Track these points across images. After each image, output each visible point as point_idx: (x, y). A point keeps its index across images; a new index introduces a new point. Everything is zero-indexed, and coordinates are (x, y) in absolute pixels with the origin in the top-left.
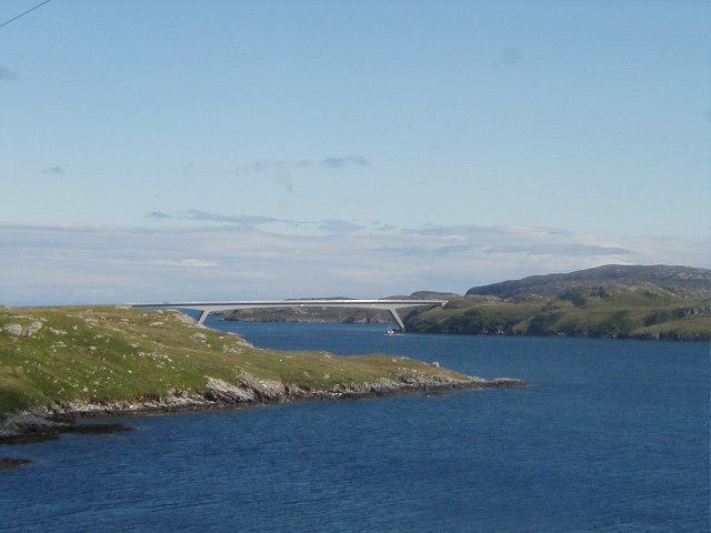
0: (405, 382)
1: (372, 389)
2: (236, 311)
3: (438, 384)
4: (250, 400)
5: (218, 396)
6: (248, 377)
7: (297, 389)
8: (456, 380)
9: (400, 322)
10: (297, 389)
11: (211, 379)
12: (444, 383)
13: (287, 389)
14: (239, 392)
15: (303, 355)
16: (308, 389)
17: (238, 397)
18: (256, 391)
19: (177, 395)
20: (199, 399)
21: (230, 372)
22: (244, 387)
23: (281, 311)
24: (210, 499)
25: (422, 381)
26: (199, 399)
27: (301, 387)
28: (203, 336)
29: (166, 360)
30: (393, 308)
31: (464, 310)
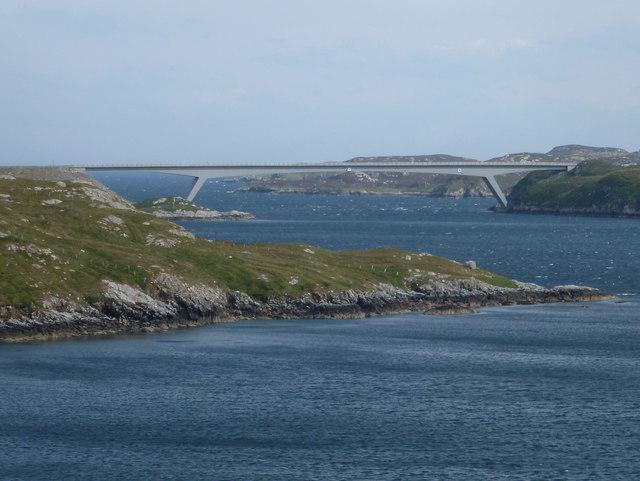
0: (417, 290)
1: (360, 301)
2: (275, 176)
3: (466, 293)
4: (169, 317)
5: (123, 309)
6: (168, 279)
7: (248, 300)
8: (493, 288)
9: (502, 197)
10: (248, 300)
11: (112, 284)
12: (475, 292)
13: (232, 300)
14: (154, 304)
15: (75, 385)
16: (264, 300)
17: (153, 312)
18: (181, 303)
19: (61, 308)
20: (94, 314)
21: (142, 273)
22: (164, 296)
23: (338, 177)
24: (381, 173)
25: (442, 288)
26: (94, 314)
27: (254, 296)
28: (118, 221)
29: (47, 258)
30: (490, 174)
31: (599, 177)
